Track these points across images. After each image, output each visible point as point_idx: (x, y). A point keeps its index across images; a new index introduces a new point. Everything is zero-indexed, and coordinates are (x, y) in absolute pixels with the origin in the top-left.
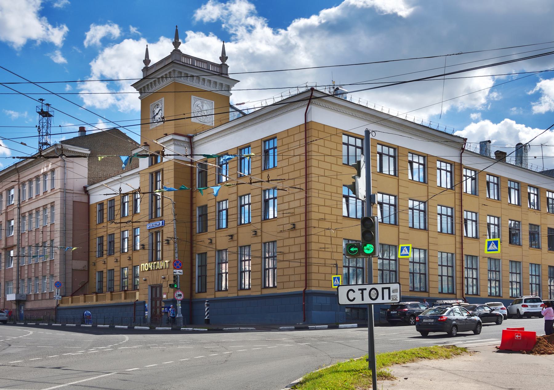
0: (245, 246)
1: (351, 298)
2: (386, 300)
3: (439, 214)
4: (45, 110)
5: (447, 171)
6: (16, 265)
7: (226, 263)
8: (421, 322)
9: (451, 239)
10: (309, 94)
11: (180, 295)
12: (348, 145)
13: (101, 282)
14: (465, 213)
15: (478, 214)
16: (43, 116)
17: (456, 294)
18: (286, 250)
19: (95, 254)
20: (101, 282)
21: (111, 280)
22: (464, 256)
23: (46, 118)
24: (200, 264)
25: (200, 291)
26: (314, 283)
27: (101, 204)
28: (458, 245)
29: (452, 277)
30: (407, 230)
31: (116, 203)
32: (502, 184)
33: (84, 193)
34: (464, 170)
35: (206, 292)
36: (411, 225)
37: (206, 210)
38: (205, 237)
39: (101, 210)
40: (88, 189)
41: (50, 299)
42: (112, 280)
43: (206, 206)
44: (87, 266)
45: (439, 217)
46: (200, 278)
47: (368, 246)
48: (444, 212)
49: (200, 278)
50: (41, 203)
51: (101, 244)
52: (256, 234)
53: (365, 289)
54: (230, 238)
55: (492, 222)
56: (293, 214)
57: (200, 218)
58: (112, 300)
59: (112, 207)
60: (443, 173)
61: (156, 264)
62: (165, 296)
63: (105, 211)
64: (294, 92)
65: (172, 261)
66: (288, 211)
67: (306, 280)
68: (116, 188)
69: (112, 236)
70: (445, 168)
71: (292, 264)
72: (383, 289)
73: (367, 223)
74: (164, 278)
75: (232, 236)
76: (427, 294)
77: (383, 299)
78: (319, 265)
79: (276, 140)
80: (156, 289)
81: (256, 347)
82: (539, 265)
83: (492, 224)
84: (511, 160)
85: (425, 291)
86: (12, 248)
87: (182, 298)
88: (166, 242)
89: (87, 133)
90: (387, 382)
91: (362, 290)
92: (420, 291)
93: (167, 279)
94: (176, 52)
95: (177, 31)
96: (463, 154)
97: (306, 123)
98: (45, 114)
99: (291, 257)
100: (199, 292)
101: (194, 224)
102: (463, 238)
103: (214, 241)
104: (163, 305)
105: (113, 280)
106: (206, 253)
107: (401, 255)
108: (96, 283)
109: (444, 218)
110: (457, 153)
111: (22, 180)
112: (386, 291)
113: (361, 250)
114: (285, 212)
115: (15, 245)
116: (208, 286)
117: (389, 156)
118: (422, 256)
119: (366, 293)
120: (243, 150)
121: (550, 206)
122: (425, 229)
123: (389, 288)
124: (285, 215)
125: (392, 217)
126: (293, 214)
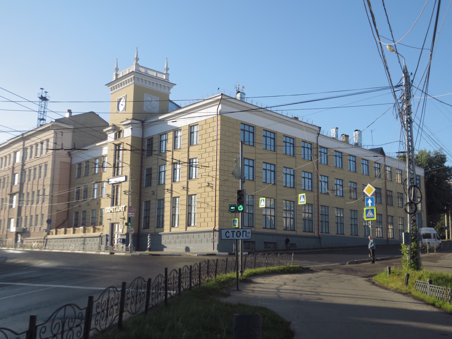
1: (228, 236)
3: (303, 177)
4: (44, 96)
7: (407, 203)
8: (441, 166)
21: (189, 205)
27: (80, 164)
28: (316, 199)
32: (344, 157)
33: (68, 156)
35: (149, 228)
36: (264, 181)
37: (152, 141)
39: (80, 169)
43: (151, 168)
45: (284, 220)
47: (241, 206)
48: (307, 176)
50: (37, 162)
61: (116, 208)
65: (127, 205)
68: (268, 268)
73: (240, 200)
77: (243, 236)
79: (198, 126)
81: (448, 220)
82: (328, 207)
85: (294, 230)
87: (133, 232)
90: (64, 145)
92: (291, 230)
94: (218, 231)
96: (74, 314)
100: (144, 228)
103: (155, 193)
106: (150, 201)
107: (367, 218)
109: (307, 180)
111: (26, 146)
112: (245, 233)
113: (236, 209)
116: (151, 224)
118: (272, 203)
119: (235, 233)
120: (192, 127)
122: (294, 188)
125: (273, 180)
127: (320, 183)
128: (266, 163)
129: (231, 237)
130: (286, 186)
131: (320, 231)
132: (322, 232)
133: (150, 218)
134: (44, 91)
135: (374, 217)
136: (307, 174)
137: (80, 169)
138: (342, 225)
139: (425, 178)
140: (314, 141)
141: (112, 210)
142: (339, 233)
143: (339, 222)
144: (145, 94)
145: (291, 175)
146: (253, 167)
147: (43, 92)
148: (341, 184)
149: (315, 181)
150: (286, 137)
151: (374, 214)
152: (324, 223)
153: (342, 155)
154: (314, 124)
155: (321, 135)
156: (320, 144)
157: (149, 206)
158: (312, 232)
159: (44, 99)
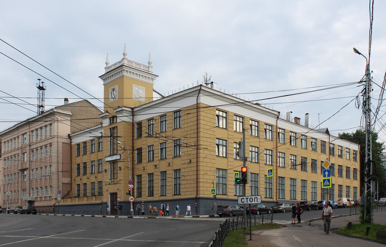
0: (150, 146)
2: (256, 202)
4: (41, 86)
5: (240, 122)
6: (28, 180)
9: (271, 143)
10: (199, 88)
11: (132, 199)
12: (236, 121)
13: (79, 190)
14: (278, 153)
15: (285, 154)
16: (40, 90)
17: (273, 198)
18: (186, 174)
19: (75, 174)
20: (79, 190)
22: (278, 177)
23: (42, 91)
24: (138, 181)
25: (149, 195)
26: (201, 192)
27: (78, 145)
29: (272, 156)
30: (233, 160)
31: (87, 145)
33: (68, 138)
34: (278, 129)
35: (141, 197)
38: (140, 166)
39: (79, 148)
40: (71, 136)
41: (49, 200)
42: (85, 190)
44: (70, 181)
46: (175, 186)
48: (268, 153)
49: (138, 189)
51: (79, 168)
52: (169, 165)
53: (248, 198)
54: (155, 166)
55: (313, 141)
56: (190, 155)
57: (138, 155)
58: (87, 201)
59: (85, 147)
60: (238, 123)
62: (118, 199)
63: (81, 149)
64: (16, 123)
66: (187, 153)
67: (197, 191)
69: (85, 164)
70: (239, 120)
71: (189, 182)
72: (255, 198)
73: (244, 174)
74: (118, 189)
75: (156, 166)
76: (273, 199)
77: (255, 202)
78: (204, 182)
80: (114, 195)
82: (316, 182)
83: (292, 136)
84: (302, 122)
86: (25, 169)
88: (119, 168)
89: (69, 102)
91: (247, 198)
93: (120, 189)
95: (360, 54)
96: (278, 120)
97: (197, 104)
98: (41, 88)
99: (189, 178)
101: (134, 154)
102: (278, 167)
104: (118, 204)
105: (80, 190)
106: (142, 175)
107: (324, 186)
108: (75, 191)
109: (268, 156)
110: (275, 120)
112: (256, 199)
114: (186, 153)
115: (28, 168)
116: (87, 172)
117: (223, 117)
119: (248, 200)
121: (339, 172)
122: (226, 157)
123: (257, 198)
124: (186, 155)
126: (190, 155)
127: (278, 158)
128: (252, 146)
129: (245, 203)
130: (219, 156)
131: (278, 197)
132: (279, 198)
133: (142, 189)
134: (41, 81)
135: (329, 186)
136: (254, 148)
137: (79, 148)
138: (305, 193)
139: (360, 153)
140: (274, 124)
141: (110, 182)
142: (268, 196)
143: (281, 188)
144: (133, 85)
145: (270, 155)
146: (226, 146)
147: (40, 83)
148: (283, 157)
149: (274, 157)
150: (266, 125)
151: (330, 183)
152: (281, 191)
153: (306, 139)
154: (274, 109)
155: (280, 118)
156: (279, 126)
157: (141, 179)
158: (272, 198)
159: (41, 88)
